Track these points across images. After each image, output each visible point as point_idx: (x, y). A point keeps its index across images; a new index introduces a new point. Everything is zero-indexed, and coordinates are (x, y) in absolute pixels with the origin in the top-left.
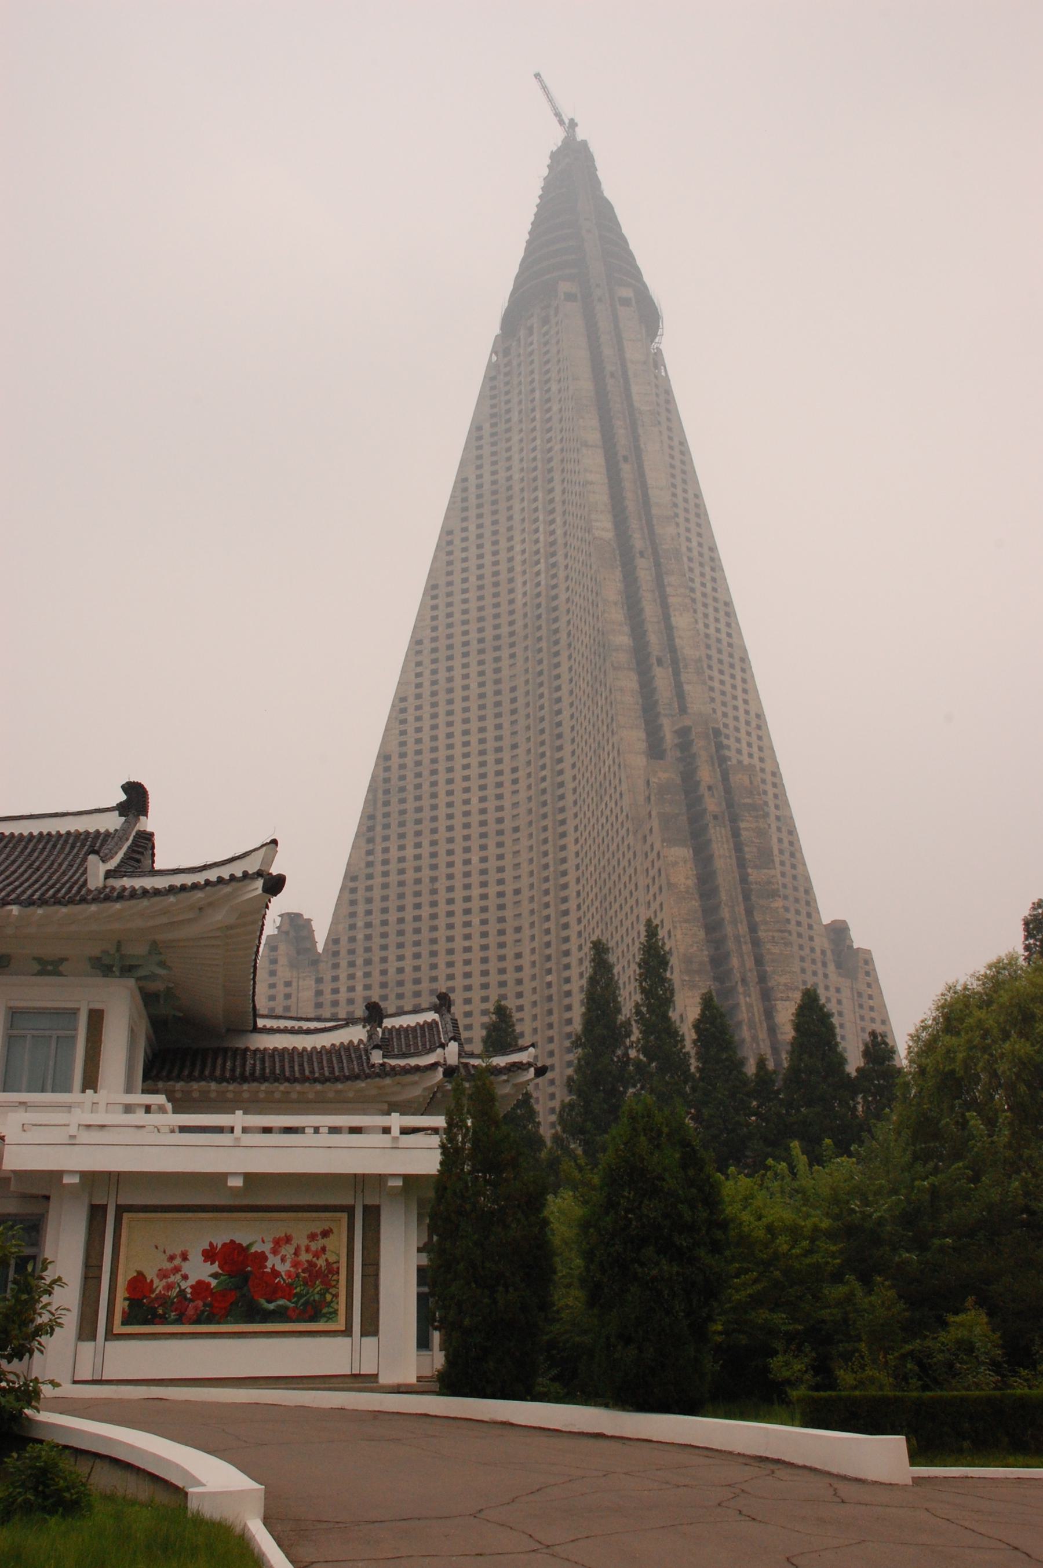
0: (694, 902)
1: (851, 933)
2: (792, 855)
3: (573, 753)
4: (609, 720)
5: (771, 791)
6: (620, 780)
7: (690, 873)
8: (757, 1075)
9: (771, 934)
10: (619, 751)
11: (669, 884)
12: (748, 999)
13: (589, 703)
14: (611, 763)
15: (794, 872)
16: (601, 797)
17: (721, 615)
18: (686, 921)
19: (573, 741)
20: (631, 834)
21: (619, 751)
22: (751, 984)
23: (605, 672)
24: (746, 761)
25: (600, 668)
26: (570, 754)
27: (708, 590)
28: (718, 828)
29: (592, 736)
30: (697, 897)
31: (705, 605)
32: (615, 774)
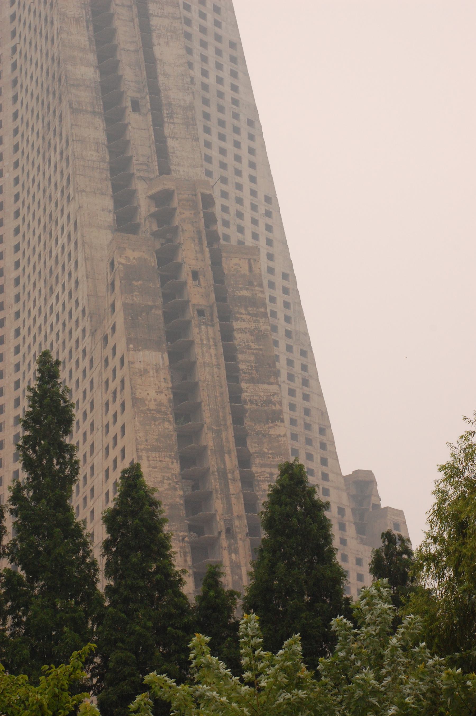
0: (166, 424)
1: (378, 488)
2: (305, 382)
3: (17, 231)
4: (65, 183)
5: (280, 298)
6: (76, 263)
7: (163, 384)
8: (202, 598)
9: (268, 470)
10: (75, 224)
11: (135, 401)
12: (233, 556)
13: (39, 161)
14: (66, 240)
15: (306, 404)
16: (51, 288)
17: (225, 60)
18: (155, 449)
19: (17, 214)
20: (88, 334)
21: (75, 224)
22: (239, 536)
23: (61, 116)
24: (249, 241)
25: (54, 112)
26: (12, 232)
27: (209, 24)
28: (203, 327)
29: (42, 207)
30: (171, 417)
31: (204, 44)
32: (69, 255)
